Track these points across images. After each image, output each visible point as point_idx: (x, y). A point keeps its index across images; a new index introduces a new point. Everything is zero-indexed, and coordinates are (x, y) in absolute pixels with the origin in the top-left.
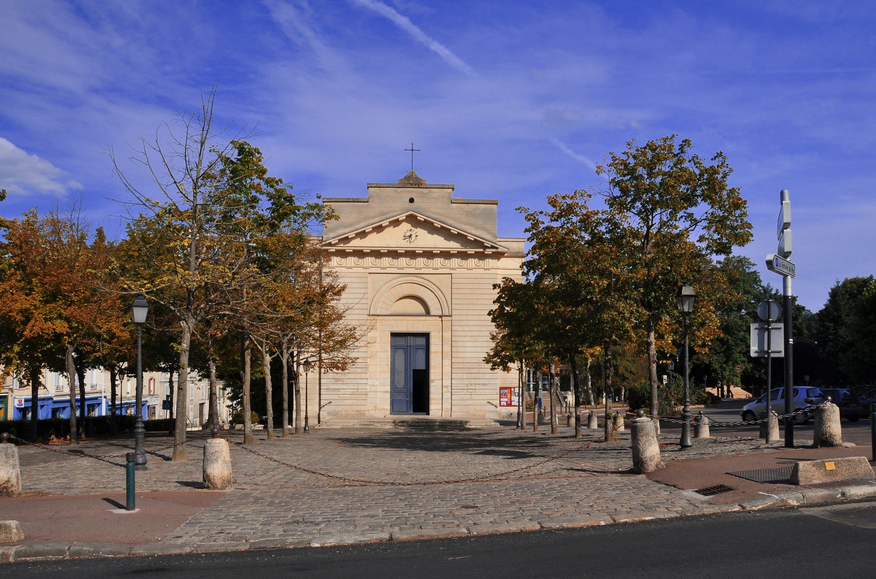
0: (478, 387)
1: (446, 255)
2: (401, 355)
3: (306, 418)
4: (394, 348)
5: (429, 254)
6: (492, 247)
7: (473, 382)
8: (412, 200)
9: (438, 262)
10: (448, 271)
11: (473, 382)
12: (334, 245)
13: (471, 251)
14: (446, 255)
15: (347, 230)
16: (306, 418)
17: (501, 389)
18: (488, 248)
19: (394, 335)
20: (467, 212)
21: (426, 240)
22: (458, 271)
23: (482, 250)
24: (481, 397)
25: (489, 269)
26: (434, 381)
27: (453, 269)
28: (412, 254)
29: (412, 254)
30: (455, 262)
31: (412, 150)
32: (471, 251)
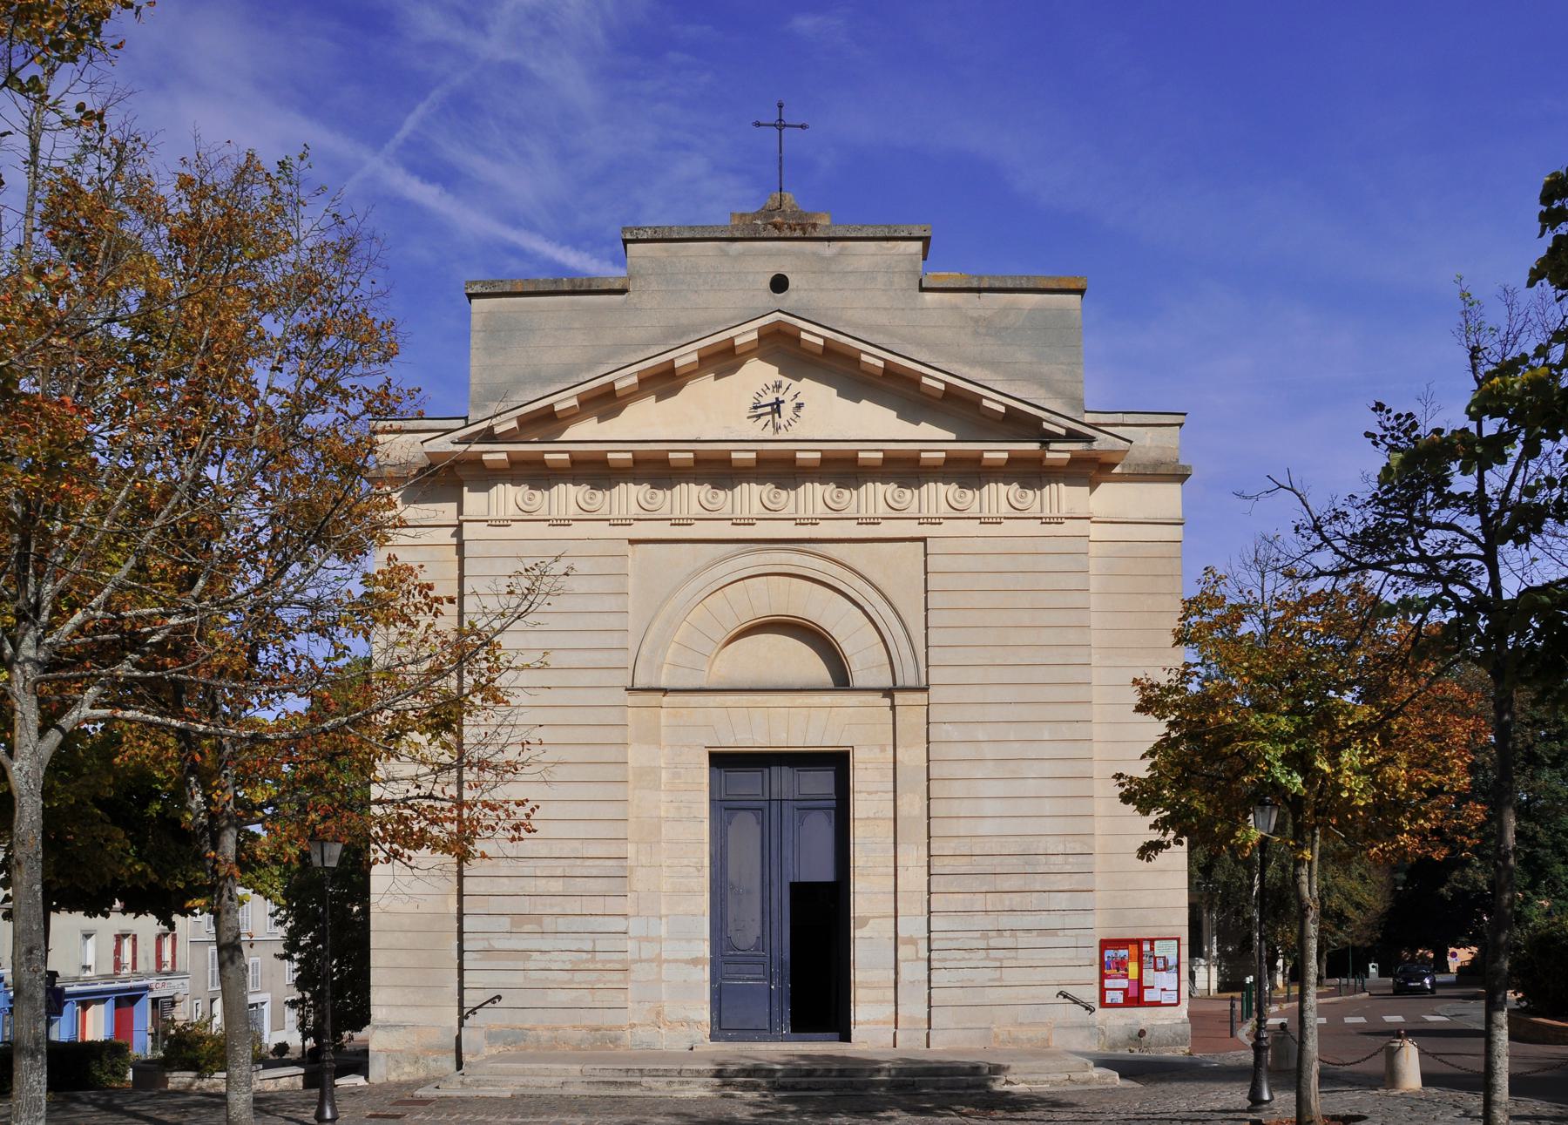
0: (1024, 940)
1: (905, 469)
2: (747, 832)
4: (723, 808)
5: (843, 469)
6: (1072, 436)
7: (1006, 921)
8: (779, 284)
9: (876, 496)
11: (1006, 921)
17: (1105, 944)
18: (1057, 438)
19: (721, 761)
20: (976, 321)
21: (828, 417)
22: (948, 528)
23: (1035, 446)
24: (1037, 976)
26: (865, 921)
28: (781, 469)
30: (938, 496)
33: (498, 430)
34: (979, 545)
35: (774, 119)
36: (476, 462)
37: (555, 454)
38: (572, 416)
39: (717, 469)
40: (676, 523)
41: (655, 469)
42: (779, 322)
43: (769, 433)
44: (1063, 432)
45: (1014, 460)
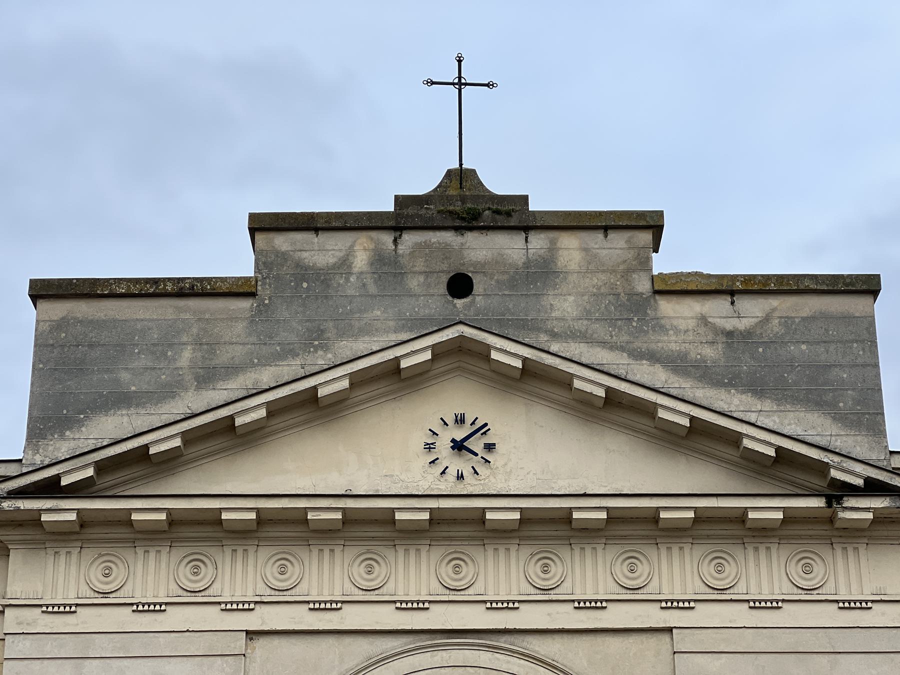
1: (633, 527)
3: (721, 317)
5: (548, 527)
6: (873, 488)
9: (590, 573)
10: (655, 617)
12: (78, 490)
13: (768, 509)
14: (633, 527)
15: (141, 422)
16: (721, 317)
20: (730, 334)
21: (540, 458)
22: (704, 615)
23: (817, 503)
25: (863, 605)
27: (671, 605)
28: (457, 528)
29: (457, 528)
30: (676, 572)
31: (460, 84)
32: (768, 509)
33: (64, 482)
34: (747, 641)
35: (452, 77)
36: (33, 521)
37: (147, 511)
38: (170, 462)
39: (368, 527)
40: (583, 605)
41: (283, 527)
42: (462, 337)
43: (448, 485)
44: (860, 482)
45: (791, 518)
